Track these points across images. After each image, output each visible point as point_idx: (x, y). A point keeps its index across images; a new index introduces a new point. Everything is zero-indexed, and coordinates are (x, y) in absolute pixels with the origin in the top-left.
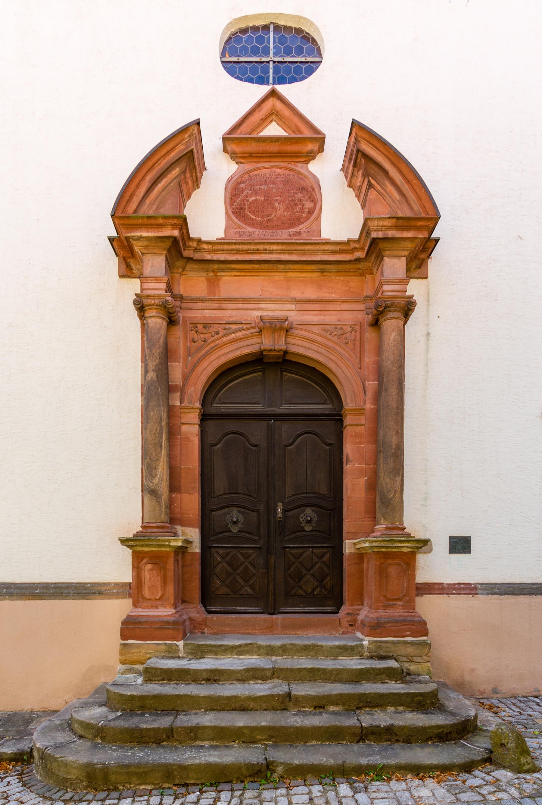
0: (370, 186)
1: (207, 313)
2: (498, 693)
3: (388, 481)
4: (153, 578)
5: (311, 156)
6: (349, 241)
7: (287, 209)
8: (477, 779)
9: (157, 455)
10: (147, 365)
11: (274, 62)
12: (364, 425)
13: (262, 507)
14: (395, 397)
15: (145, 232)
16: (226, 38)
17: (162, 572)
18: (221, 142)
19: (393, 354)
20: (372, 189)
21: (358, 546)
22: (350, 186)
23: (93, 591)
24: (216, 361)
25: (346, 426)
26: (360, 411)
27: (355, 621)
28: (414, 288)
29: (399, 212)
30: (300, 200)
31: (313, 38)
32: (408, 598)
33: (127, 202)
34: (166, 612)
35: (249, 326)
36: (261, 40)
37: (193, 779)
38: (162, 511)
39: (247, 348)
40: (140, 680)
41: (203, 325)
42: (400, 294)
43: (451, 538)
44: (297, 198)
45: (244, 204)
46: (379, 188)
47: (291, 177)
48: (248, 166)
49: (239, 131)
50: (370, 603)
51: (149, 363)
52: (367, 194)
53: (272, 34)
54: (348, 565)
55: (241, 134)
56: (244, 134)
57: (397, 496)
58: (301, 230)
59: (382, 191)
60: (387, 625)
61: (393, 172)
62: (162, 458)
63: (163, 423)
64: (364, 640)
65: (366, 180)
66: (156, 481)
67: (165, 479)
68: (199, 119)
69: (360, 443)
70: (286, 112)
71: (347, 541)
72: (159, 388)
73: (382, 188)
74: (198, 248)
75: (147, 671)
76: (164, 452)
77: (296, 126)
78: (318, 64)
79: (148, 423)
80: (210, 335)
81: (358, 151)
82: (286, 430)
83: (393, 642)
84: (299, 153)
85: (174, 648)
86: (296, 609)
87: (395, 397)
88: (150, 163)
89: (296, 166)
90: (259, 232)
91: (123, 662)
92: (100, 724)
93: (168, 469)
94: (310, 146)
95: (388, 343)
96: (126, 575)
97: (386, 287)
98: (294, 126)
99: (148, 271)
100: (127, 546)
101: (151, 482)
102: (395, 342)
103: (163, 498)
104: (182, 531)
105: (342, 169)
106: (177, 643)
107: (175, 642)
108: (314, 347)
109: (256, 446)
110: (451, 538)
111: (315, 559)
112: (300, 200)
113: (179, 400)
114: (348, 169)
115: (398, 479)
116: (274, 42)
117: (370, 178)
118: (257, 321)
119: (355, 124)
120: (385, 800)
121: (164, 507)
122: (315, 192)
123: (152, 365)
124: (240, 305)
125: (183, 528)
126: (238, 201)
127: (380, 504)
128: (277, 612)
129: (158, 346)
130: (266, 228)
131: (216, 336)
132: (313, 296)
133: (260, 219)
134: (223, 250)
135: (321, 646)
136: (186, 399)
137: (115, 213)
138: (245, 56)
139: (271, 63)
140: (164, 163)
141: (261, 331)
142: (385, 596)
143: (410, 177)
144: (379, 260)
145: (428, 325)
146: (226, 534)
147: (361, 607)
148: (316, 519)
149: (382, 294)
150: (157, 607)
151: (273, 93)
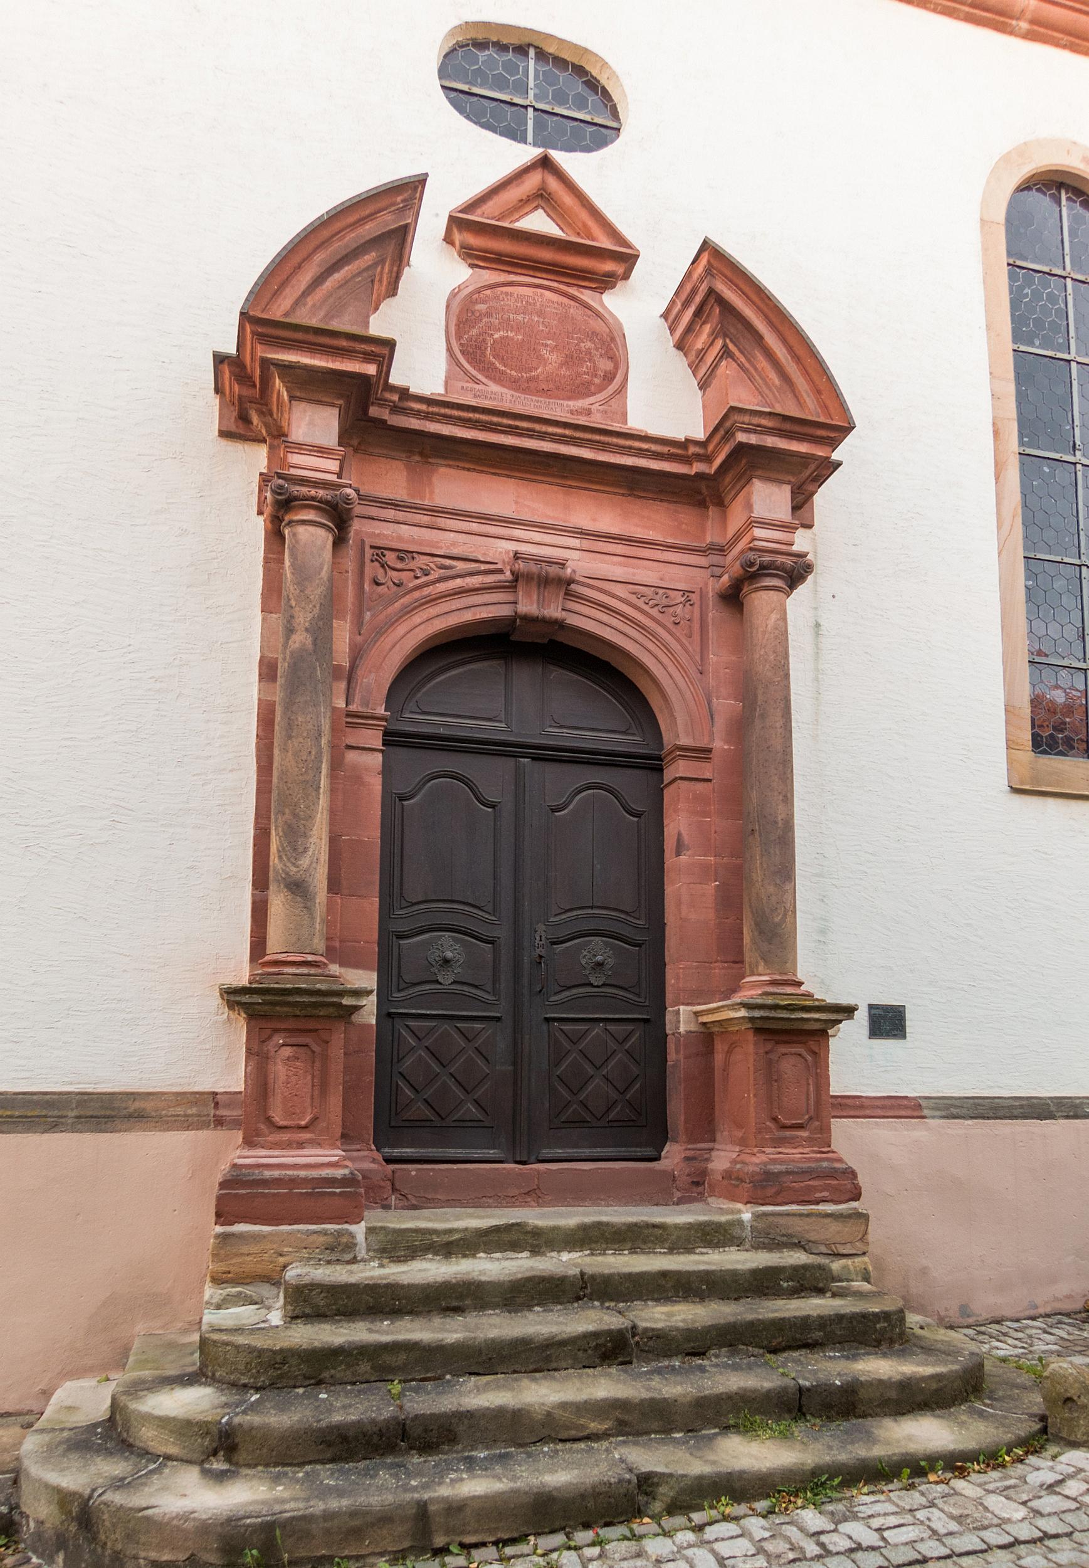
0: (726, 353)
1: (387, 530)
2: (968, 1316)
3: (771, 889)
4: (294, 1079)
5: (605, 283)
6: (688, 442)
8: (1041, 1472)
9: (308, 807)
10: (292, 617)
11: (535, 109)
12: (709, 780)
13: (503, 933)
14: (779, 731)
15: (306, 357)
16: (446, 50)
17: (318, 1065)
19: (774, 652)
21: (705, 1019)
22: (680, 346)
23: (125, 1112)
24: (423, 626)
26: (703, 753)
27: (704, 1173)
28: (801, 541)
31: (603, 88)
34: (323, 1159)
35: (492, 567)
36: (511, 68)
37: (476, 1532)
39: (490, 608)
40: (276, 1318)
42: (784, 547)
45: (484, 340)
46: (743, 360)
48: (489, 276)
49: (479, 211)
51: (296, 615)
53: (532, 63)
55: (482, 216)
58: (592, 407)
59: (747, 365)
60: (784, 1179)
61: (771, 339)
63: (324, 741)
65: (719, 343)
66: (305, 862)
68: (427, 175)
69: (707, 814)
70: (568, 200)
73: (748, 360)
74: (400, 405)
77: (585, 225)
79: (290, 737)
80: (412, 574)
81: (711, 291)
84: (589, 272)
85: (344, 1240)
92: (224, 1420)
94: (609, 266)
95: (764, 632)
96: (229, 1075)
98: (580, 225)
99: (301, 431)
103: (317, 901)
105: (665, 316)
106: (352, 1228)
107: (346, 1226)
108: (615, 622)
111: (612, 1045)
112: (588, 352)
116: (536, 77)
117: (728, 341)
120: (903, 1529)
122: (616, 345)
124: (474, 527)
126: (470, 333)
127: (756, 933)
128: (533, 1158)
130: (526, 391)
131: (424, 579)
132: (614, 530)
134: (450, 417)
135: (661, 1226)
136: (357, 698)
138: (481, 86)
139: (530, 110)
140: (351, 239)
141: (517, 581)
142: (775, 1120)
143: (801, 351)
145: (816, 609)
146: (428, 987)
147: (710, 1145)
148: (611, 961)
150: (301, 1145)
151: (545, 163)
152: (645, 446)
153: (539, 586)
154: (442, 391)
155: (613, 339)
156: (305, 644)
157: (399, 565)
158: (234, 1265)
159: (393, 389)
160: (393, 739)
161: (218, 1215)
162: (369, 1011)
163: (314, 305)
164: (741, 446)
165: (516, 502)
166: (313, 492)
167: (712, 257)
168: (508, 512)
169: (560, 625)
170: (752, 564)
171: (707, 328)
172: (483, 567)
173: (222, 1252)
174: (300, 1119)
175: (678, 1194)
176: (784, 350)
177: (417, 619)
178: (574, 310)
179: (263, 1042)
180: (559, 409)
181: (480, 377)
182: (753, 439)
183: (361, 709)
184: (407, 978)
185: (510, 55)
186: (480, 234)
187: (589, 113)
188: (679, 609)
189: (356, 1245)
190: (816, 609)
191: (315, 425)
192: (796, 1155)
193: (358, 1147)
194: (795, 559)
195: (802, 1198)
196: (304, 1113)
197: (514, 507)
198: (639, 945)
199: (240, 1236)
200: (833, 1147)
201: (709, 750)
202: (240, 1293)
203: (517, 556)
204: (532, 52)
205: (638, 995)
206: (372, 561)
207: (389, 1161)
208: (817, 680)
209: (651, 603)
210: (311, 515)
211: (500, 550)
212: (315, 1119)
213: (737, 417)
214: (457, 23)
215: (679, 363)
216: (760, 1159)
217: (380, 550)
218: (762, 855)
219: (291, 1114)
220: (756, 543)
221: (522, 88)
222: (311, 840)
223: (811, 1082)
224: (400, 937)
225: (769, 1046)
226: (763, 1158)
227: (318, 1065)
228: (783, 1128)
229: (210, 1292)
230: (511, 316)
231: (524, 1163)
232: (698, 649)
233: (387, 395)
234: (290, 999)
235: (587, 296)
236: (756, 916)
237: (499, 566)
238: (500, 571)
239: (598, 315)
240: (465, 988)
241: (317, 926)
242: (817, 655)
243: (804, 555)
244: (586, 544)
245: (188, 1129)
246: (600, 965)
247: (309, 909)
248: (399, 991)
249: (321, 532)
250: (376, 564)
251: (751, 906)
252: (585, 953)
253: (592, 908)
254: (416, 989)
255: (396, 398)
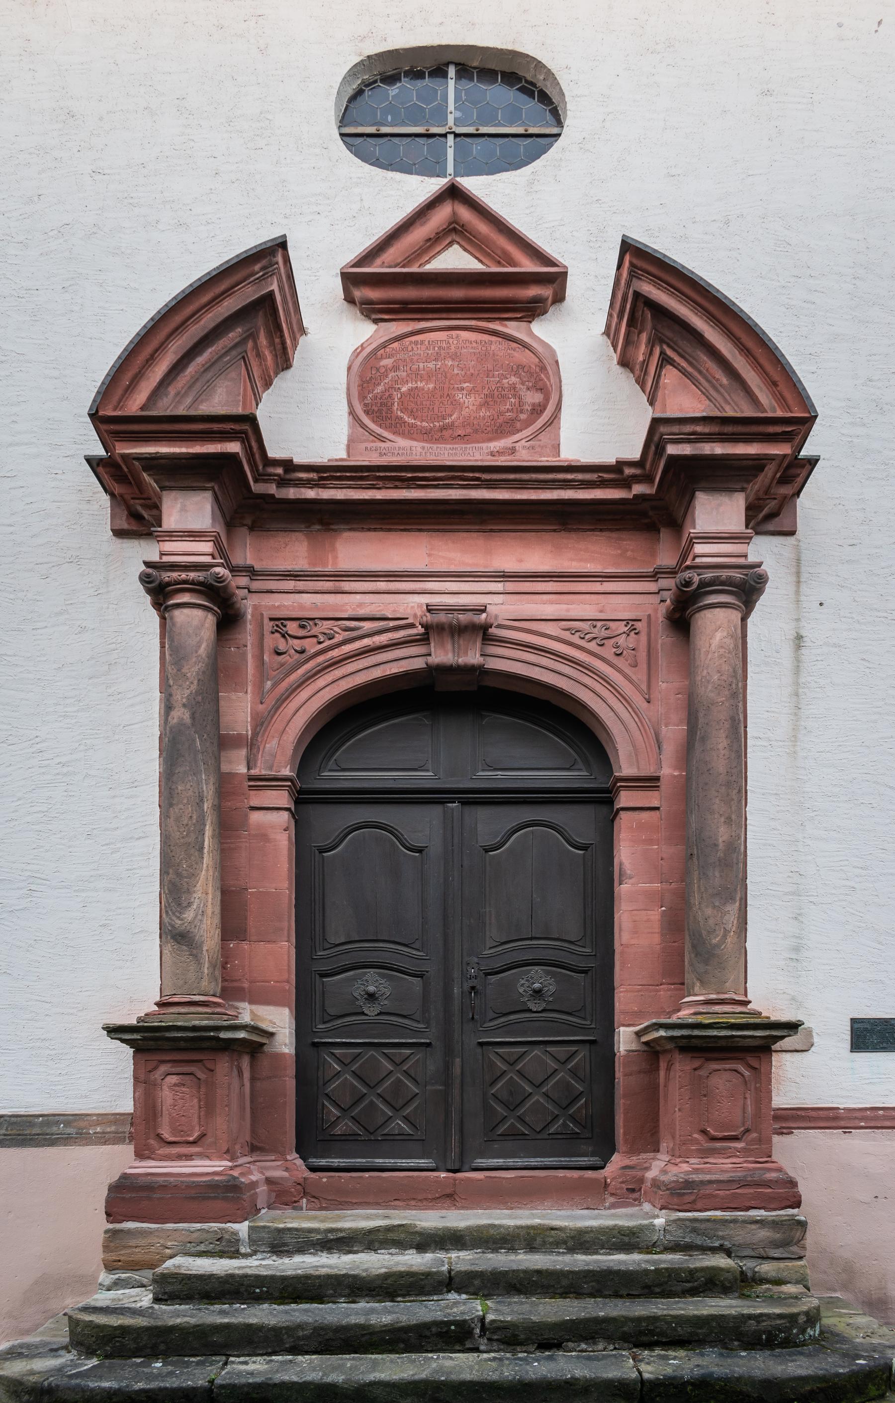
3: (709, 911)
4: (181, 1102)
5: (532, 310)
6: (621, 465)
7: (485, 404)
9: (191, 866)
10: (171, 695)
11: (457, 135)
12: (657, 809)
14: (723, 752)
16: (350, 91)
18: (339, 281)
20: (669, 367)
21: (645, 1039)
24: (327, 689)
25: (619, 810)
26: (650, 782)
27: (642, 1180)
29: (727, 408)
30: (515, 388)
32: (755, 1135)
33: (126, 390)
38: (203, 973)
41: (298, 622)
43: (854, 1021)
44: (506, 385)
45: (390, 396)
46: (684, 364)
47: (493, 347)
49: (378, 261)
50: (671, 1145)
51: (174, 693)
52: (659, 376)
53: (451, 83)
54: (625, 1075)
56: (390, 267)
57: (729, 940)
59: (690, 369)
62: (204, 872)
64: (658, 1217)
65: (657, 351)
66: (189, 915)
67: (209, 911)
68: (285, 236)
69: (651, 842)
70: (483, 228)
71: (622, 1029)
72: (193, 740)
73: (690, 363)
74: (288, 477)
75: (162, 1280)
76: (207, 860)
78: (553, 139)
80: (315, 640)
81: (637, 295)
82: (488, 823)
83: (724, 1222)
86: (510, 1162)
87: (723, 752)
88: (178, 319)
89: (506, 326)
90: (423, 448)
91: (110, 1267)
93: (219, 894)
94: (533, 291)
97: (699, 549)
99: (173, 519)
100: (123, 1041)
101: (178, 918)
102: (722, 650)
103: (205, 948)
104: (252, 1012)
105: (607, 333)
109: (420, 851)
110: (854, 1021)
112: (513, 387)
113: (245, 763)
114: (617, 330)
115: (733, 908)
117: (665, 347)
118: (419, 613)
119: (628, 247)
121: (206, 965)
123: (181, 695)
124: (382, 585)
125: (254, 1007)
127: (693, 955)
128: (466, 1167)
129: (194, 660)
130: (441, 440)
133: (425, 424)
137: (97, 411)
139: (451, 138)
140: (209, 320)
144: (687, 498)
145: (798, 620)
149: (694, 559)
150: (189, 1157)
151: (453, 193)
152: (569, 476)
153: (453, 636)
154: (343, 455)
155: (543, 368)
156: (183, 719)
157: (302, 633)
158: (123, 1255)
159: (276, 463)
160: (306, 799)
161: (108, 1214)
162: (285, 1042)
163: (177, 394)
164: (673, 458)
165: (429, 555)
166: (184, 576)
167: (637, 258)
168: (419, 565)
169: (479, 671)
170: (688, 583)
171: (644, 337)
172: (392, 624)
173: (112, 1244)
174: (188, 1135)
175: (612, 1200)
176: (730, 345)
177: (321, 682)
178: (496, 345)
179: (150, 1071)
180: (477, 454)
181: (386, 434)
182: (686, 450)
183: (263, 772)
184: (332, 1011)
185: (427, 81)
186: (383, 287)
187: (523, 124)
188: (621, 640)
189: (238, 1240)
190: (798, 620)
191: (190, 512)
192: (725, 1166)
193: (273, 1158)
194: (745, 571)
195: (727, 1205)
196: (192, 1130)
197: (427, 560)
198: (585, 972)
199: (129, 1232)
200: (774, 1158)
201: (657, 779)
202: (129, 1278)
203: (430, 609)
204: (452, 71)
205: (584, 1019)
206: (273, 633)
207: (313, 1169)
208: (797, 695)
209: (587, 637)
210: (186, 598)
211: (411, 605)
212: (203, 1136)
213: (663, 429)
214: (357, 59)
215: (625, 382)
216: (682, 1170)
217: (279, 621)
218: (700, 879)
219: (174, 1131)
220: (698, 560)
221: (441, 113)
222: (195, 895)
223: (748, 1096)
224: (323, 975)
225: (697, 1063)
226: (685, 1167)
227: (203, 1090)
228: (717, 1140)
229: (105, 1278)
230: (421, 365)
231: (455, 1171)
232: (645, 678)
233: (271, 470)
234: (168, 1035)
235: (512, 328)
236: (701, 937)
237: (410, 621)
238: (412, 626)
239: (525, 346)
240: (392, 1018)
241: (206, 971)
242: (797, 669)
243: (759, 565)
244: (511, 586)
245: (105, 1143)
246: (538, 993)
247: (196, 957)
248: (324, 1023)
249: (198, 613)
250: (277, 635)
251: (689, 929)
252: (523, 982)
253: (531, 939)
254: (339, 1021)
255: (280, 471)
